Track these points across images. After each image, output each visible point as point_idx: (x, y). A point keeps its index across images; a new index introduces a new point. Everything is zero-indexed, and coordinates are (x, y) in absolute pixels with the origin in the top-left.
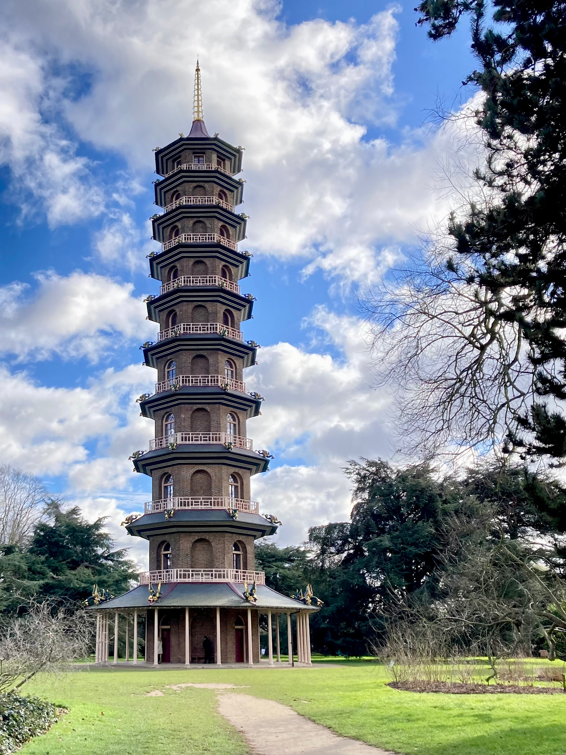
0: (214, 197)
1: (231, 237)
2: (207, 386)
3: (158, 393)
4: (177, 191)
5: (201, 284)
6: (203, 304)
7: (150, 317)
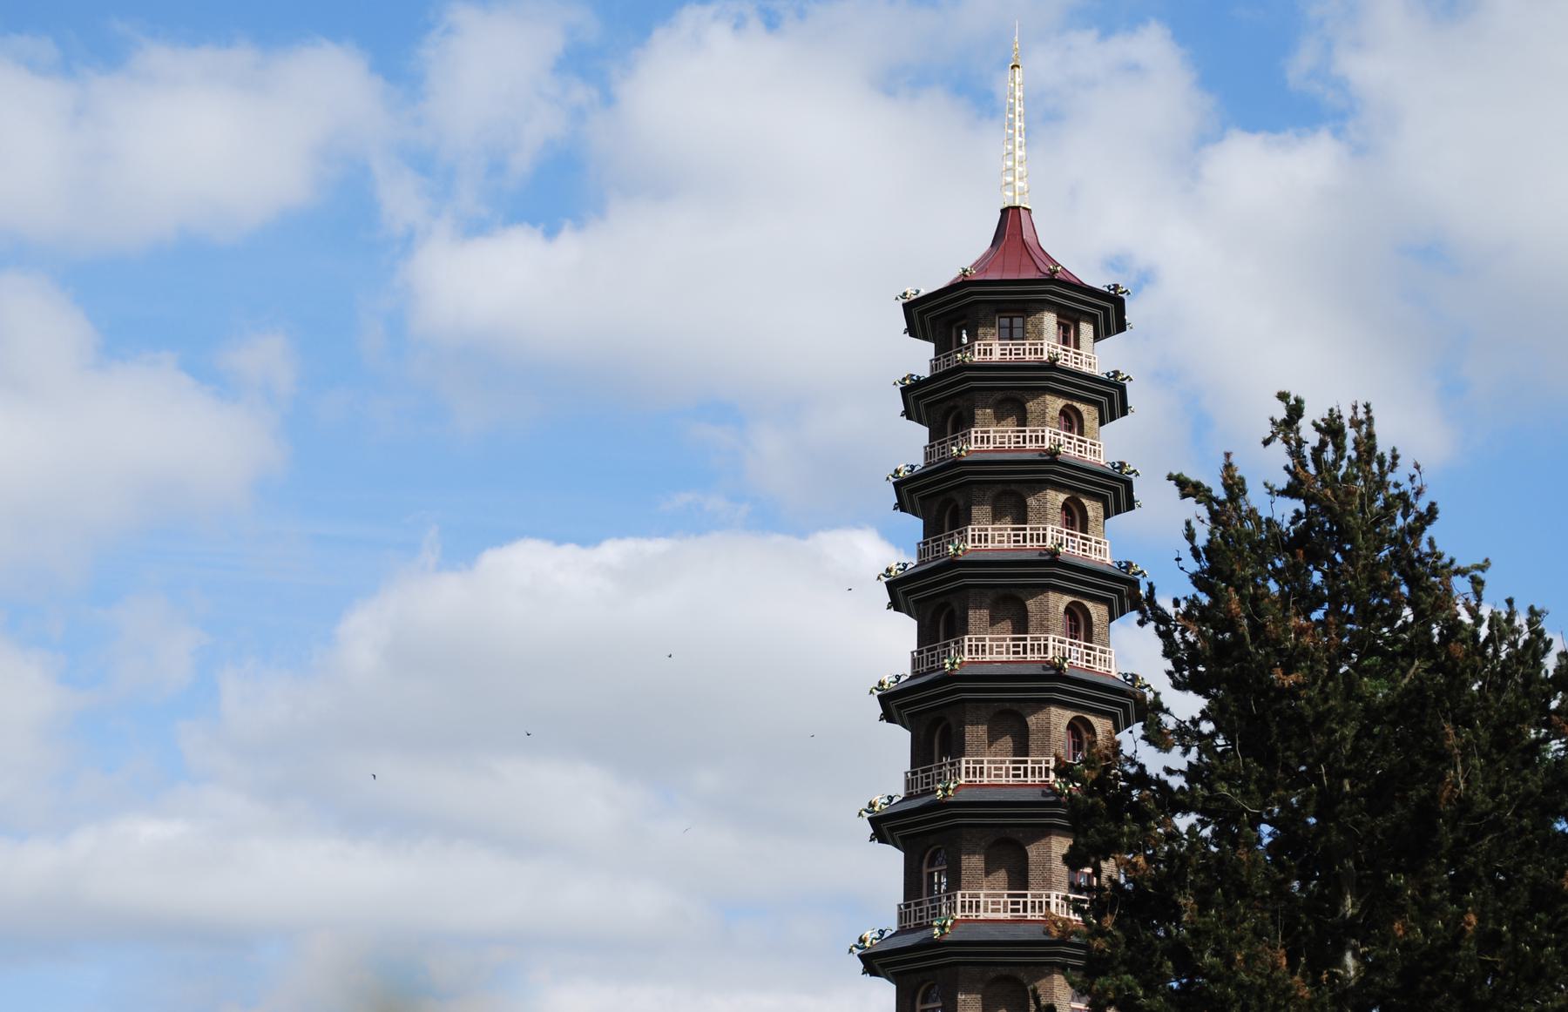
0: (1047, 429)
1: (1091, 525)
2: (1022, 450)
3: (928, 465)
4: (955, 407)
5: (1012, 545)
6: (1015, 707)
7: (907, 414)
